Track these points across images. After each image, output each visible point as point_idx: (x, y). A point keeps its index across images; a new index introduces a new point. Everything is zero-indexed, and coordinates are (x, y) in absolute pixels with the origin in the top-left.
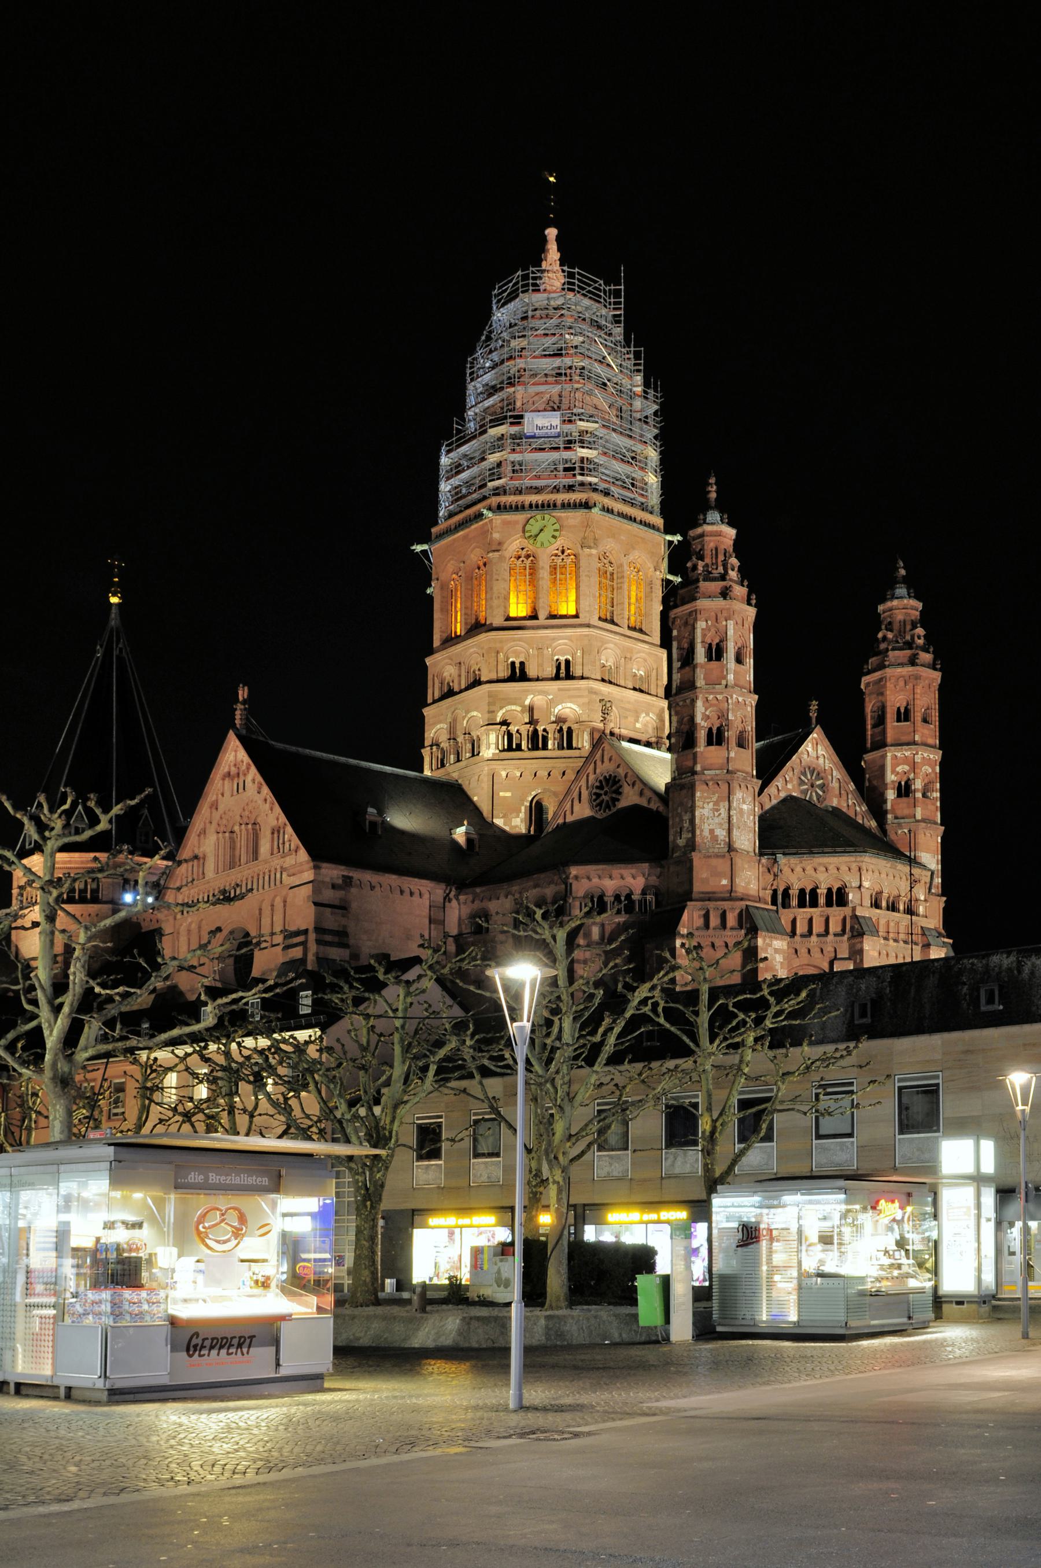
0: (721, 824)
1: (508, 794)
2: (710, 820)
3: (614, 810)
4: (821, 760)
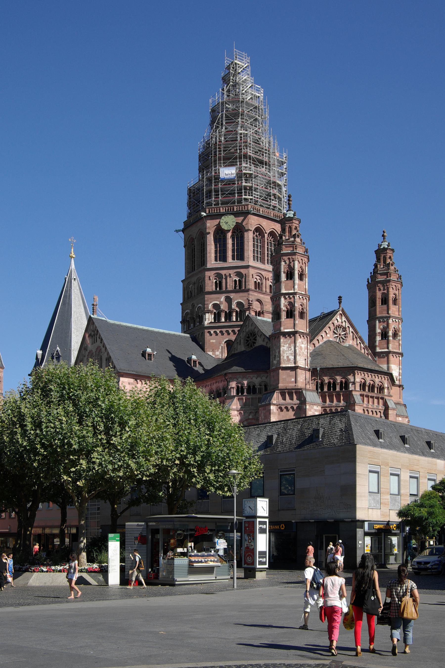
1: (214, 341)
2: (287, 352)
3: (253, 347)
4: (344, 324)
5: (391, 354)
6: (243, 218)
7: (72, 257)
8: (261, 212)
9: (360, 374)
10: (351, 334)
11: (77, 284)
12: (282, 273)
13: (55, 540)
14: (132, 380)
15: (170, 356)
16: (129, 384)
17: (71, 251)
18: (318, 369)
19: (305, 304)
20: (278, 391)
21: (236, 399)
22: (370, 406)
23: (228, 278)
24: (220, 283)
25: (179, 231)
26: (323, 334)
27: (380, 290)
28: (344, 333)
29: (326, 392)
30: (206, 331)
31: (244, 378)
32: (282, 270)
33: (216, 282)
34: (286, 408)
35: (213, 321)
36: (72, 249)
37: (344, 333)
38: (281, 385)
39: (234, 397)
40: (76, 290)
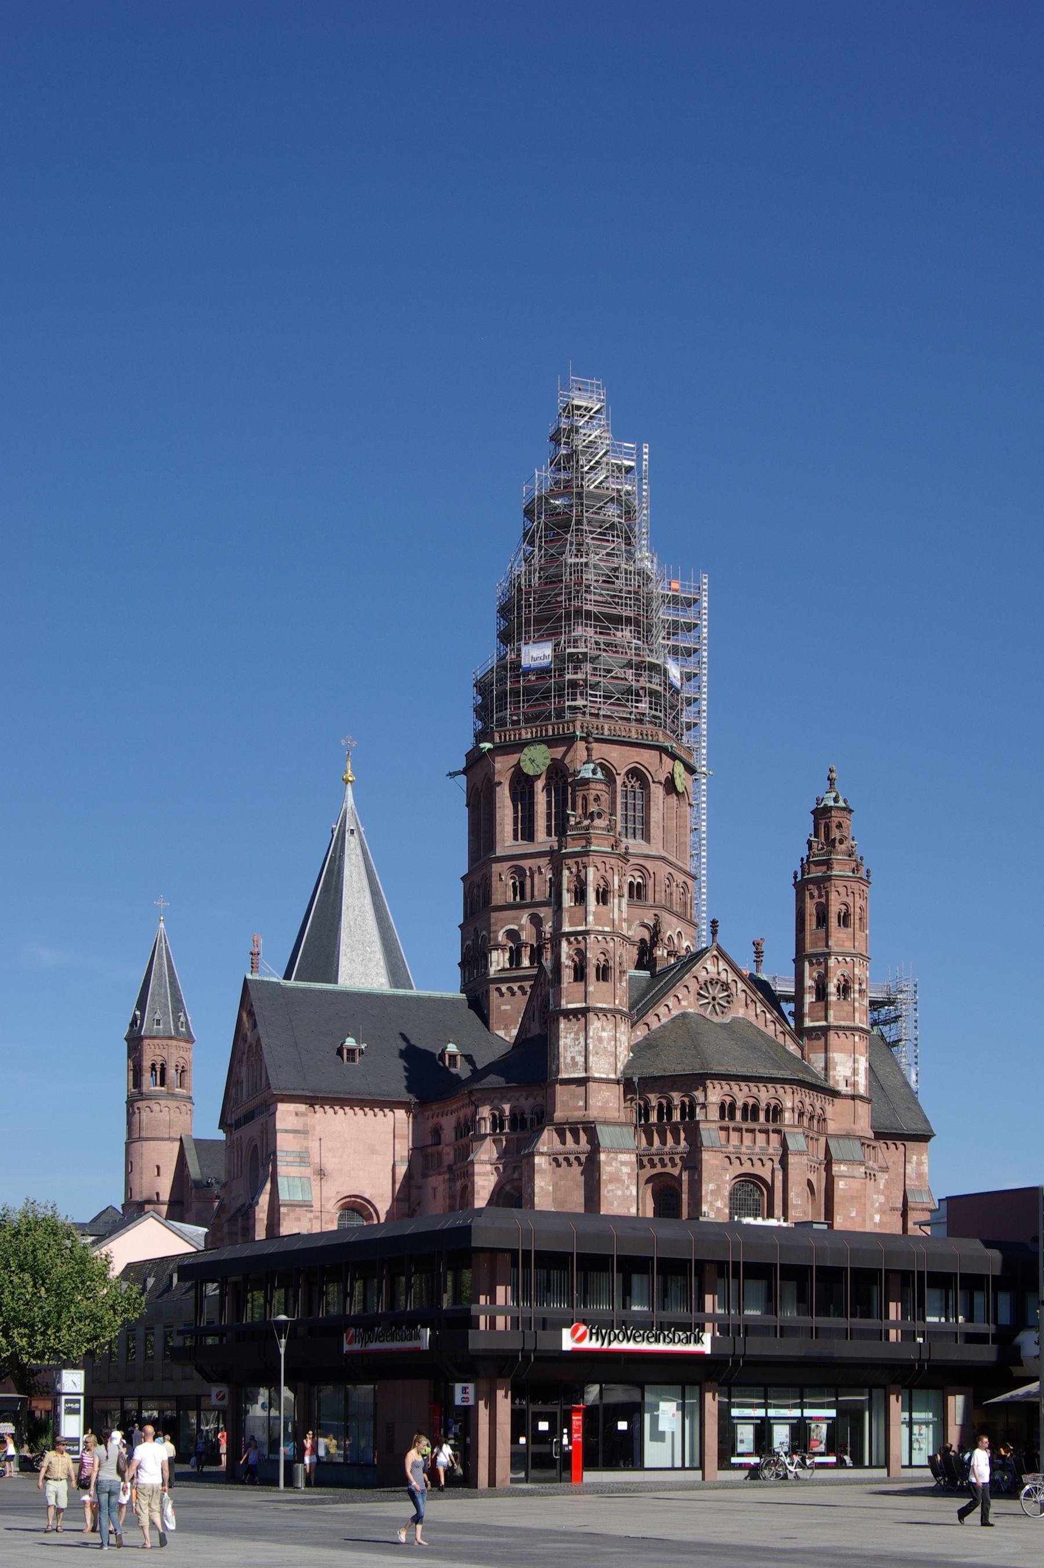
0: (580, 1052)
1: (508, 1007)
5: (832, 1032)
6: (564, 749)
7: (347, 781)
8: (606, 732)
9: (718, 1087)
10: (742, 996)
11: (358, 841)
12: (565, 892)
13: (547, 1424)
14: (302, 1107)
15: (403, 1045)
16: (297, 1114)
17: (346, 766)
18: (636, 1079)
19: (611, 950)
20: (550, 1128)
21: (489, 1140)
22: (744, 1150)
23: (536, 876)
24: (522, 885)
25: (456, 774)
26: (671, 1002)
27: (812, 897)
28: (726, 993)
29: (654, 1124)
30: (493, 987)
31: (504, 1099)
32: (565, 886)
33: (514, 884)
34: (567, 1159)
35: (508, 966)
36: (349, 764)
37: (726, 993)
38: (559, 1115)
39: (485, 1136)
40: (353, 857)
